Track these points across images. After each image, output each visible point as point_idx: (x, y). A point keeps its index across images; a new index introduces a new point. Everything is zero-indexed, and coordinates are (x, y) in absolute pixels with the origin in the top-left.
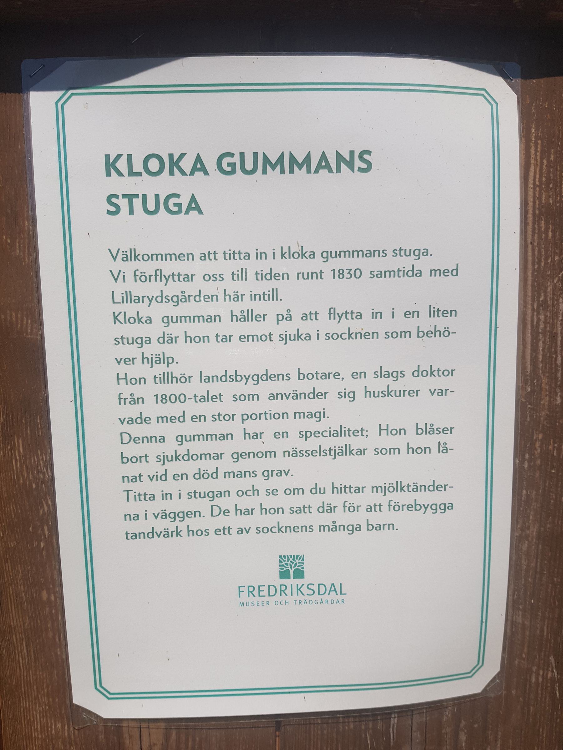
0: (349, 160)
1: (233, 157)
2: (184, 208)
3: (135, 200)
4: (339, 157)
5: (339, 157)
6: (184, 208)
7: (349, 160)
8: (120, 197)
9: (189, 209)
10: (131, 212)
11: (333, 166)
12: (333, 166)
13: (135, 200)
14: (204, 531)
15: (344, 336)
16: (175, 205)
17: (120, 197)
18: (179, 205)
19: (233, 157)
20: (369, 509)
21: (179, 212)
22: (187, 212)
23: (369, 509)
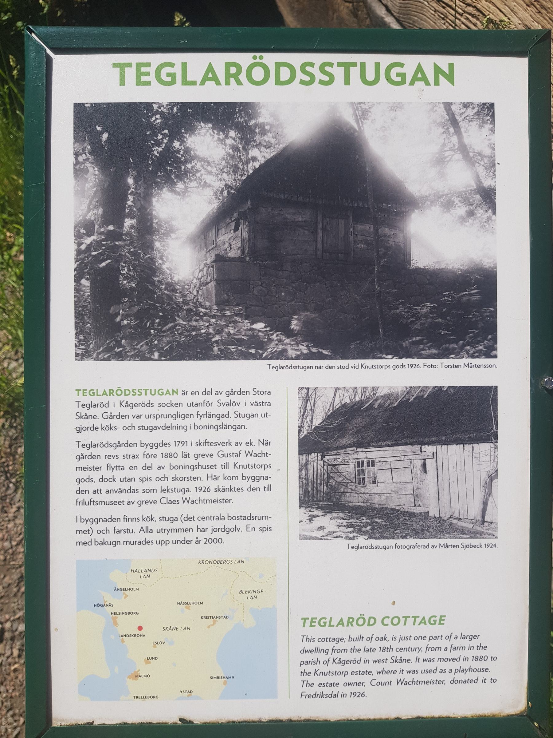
0: (448, 73)
1: (403, 67)
2: (165, 394)
3: (352, 69)
4: (173, 391)
5: (173, 391)
6: (165, 394)
7: (448, 73)
8: (335, 65)
9: (166, 394)
10: (347, 82)
11: (171, 394)
12: (171, 394)
13: (352, 69)
14: (131, 391)
15: (111, 480)
16: (398, 75)
17: (335, 65)
18: (163, 392)
19: (403, 67)
20: (95, 492)
21: (403, 82)
22: (412, 83)
23: (95, 492)
